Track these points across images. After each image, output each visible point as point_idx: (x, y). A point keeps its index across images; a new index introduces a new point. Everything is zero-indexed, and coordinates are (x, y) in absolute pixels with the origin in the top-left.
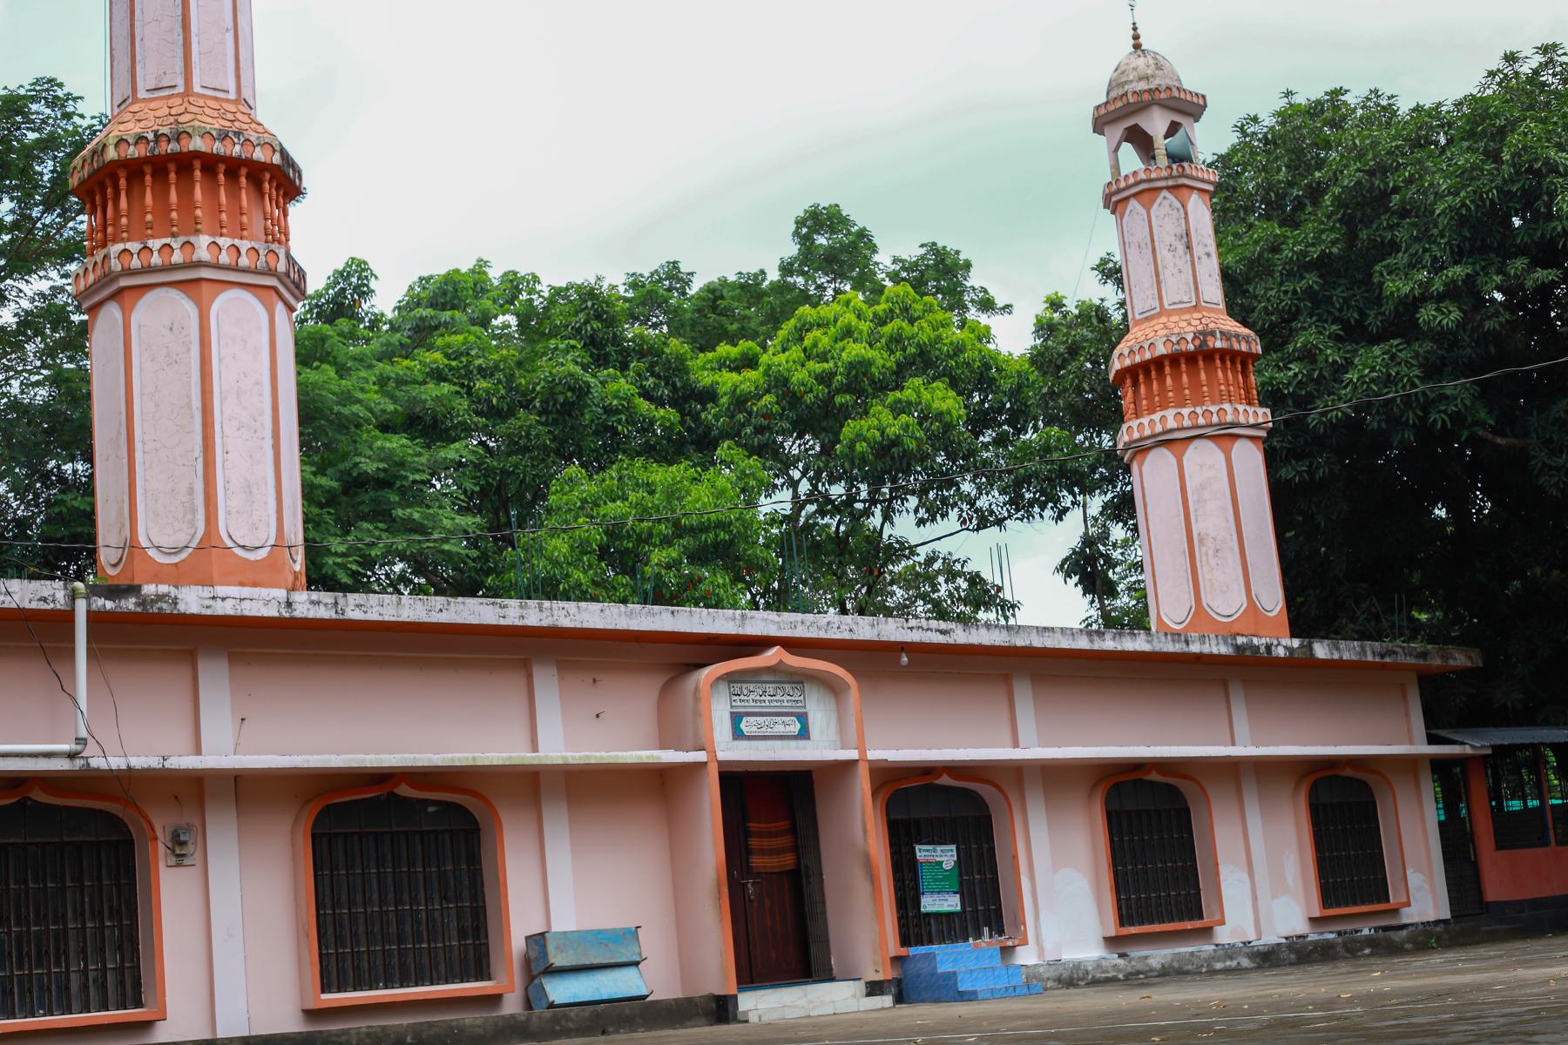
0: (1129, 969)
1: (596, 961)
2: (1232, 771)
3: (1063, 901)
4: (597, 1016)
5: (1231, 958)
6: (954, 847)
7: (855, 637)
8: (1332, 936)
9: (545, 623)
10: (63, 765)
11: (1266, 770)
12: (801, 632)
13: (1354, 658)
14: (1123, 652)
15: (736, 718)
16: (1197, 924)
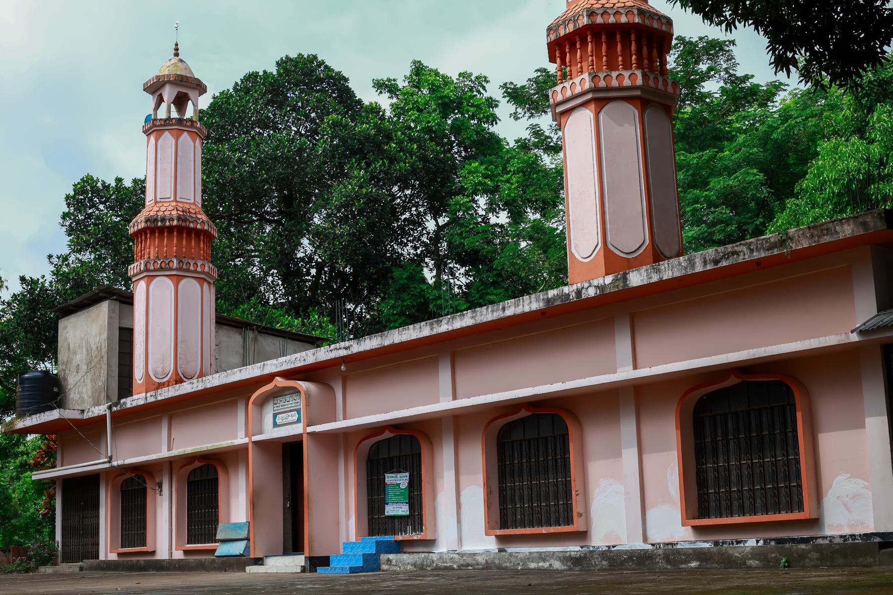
0: (462, 562)
1: (228, 537)
4: (223, 562)
5: (544, 560)
6: (407, 474)
7: (306, 363)
8: (706, 545)
9: (200, 388)
10: (107, 465)
11: (640, 396)
12: (285, 367)
13: (677, 274)
15: (275, 416)
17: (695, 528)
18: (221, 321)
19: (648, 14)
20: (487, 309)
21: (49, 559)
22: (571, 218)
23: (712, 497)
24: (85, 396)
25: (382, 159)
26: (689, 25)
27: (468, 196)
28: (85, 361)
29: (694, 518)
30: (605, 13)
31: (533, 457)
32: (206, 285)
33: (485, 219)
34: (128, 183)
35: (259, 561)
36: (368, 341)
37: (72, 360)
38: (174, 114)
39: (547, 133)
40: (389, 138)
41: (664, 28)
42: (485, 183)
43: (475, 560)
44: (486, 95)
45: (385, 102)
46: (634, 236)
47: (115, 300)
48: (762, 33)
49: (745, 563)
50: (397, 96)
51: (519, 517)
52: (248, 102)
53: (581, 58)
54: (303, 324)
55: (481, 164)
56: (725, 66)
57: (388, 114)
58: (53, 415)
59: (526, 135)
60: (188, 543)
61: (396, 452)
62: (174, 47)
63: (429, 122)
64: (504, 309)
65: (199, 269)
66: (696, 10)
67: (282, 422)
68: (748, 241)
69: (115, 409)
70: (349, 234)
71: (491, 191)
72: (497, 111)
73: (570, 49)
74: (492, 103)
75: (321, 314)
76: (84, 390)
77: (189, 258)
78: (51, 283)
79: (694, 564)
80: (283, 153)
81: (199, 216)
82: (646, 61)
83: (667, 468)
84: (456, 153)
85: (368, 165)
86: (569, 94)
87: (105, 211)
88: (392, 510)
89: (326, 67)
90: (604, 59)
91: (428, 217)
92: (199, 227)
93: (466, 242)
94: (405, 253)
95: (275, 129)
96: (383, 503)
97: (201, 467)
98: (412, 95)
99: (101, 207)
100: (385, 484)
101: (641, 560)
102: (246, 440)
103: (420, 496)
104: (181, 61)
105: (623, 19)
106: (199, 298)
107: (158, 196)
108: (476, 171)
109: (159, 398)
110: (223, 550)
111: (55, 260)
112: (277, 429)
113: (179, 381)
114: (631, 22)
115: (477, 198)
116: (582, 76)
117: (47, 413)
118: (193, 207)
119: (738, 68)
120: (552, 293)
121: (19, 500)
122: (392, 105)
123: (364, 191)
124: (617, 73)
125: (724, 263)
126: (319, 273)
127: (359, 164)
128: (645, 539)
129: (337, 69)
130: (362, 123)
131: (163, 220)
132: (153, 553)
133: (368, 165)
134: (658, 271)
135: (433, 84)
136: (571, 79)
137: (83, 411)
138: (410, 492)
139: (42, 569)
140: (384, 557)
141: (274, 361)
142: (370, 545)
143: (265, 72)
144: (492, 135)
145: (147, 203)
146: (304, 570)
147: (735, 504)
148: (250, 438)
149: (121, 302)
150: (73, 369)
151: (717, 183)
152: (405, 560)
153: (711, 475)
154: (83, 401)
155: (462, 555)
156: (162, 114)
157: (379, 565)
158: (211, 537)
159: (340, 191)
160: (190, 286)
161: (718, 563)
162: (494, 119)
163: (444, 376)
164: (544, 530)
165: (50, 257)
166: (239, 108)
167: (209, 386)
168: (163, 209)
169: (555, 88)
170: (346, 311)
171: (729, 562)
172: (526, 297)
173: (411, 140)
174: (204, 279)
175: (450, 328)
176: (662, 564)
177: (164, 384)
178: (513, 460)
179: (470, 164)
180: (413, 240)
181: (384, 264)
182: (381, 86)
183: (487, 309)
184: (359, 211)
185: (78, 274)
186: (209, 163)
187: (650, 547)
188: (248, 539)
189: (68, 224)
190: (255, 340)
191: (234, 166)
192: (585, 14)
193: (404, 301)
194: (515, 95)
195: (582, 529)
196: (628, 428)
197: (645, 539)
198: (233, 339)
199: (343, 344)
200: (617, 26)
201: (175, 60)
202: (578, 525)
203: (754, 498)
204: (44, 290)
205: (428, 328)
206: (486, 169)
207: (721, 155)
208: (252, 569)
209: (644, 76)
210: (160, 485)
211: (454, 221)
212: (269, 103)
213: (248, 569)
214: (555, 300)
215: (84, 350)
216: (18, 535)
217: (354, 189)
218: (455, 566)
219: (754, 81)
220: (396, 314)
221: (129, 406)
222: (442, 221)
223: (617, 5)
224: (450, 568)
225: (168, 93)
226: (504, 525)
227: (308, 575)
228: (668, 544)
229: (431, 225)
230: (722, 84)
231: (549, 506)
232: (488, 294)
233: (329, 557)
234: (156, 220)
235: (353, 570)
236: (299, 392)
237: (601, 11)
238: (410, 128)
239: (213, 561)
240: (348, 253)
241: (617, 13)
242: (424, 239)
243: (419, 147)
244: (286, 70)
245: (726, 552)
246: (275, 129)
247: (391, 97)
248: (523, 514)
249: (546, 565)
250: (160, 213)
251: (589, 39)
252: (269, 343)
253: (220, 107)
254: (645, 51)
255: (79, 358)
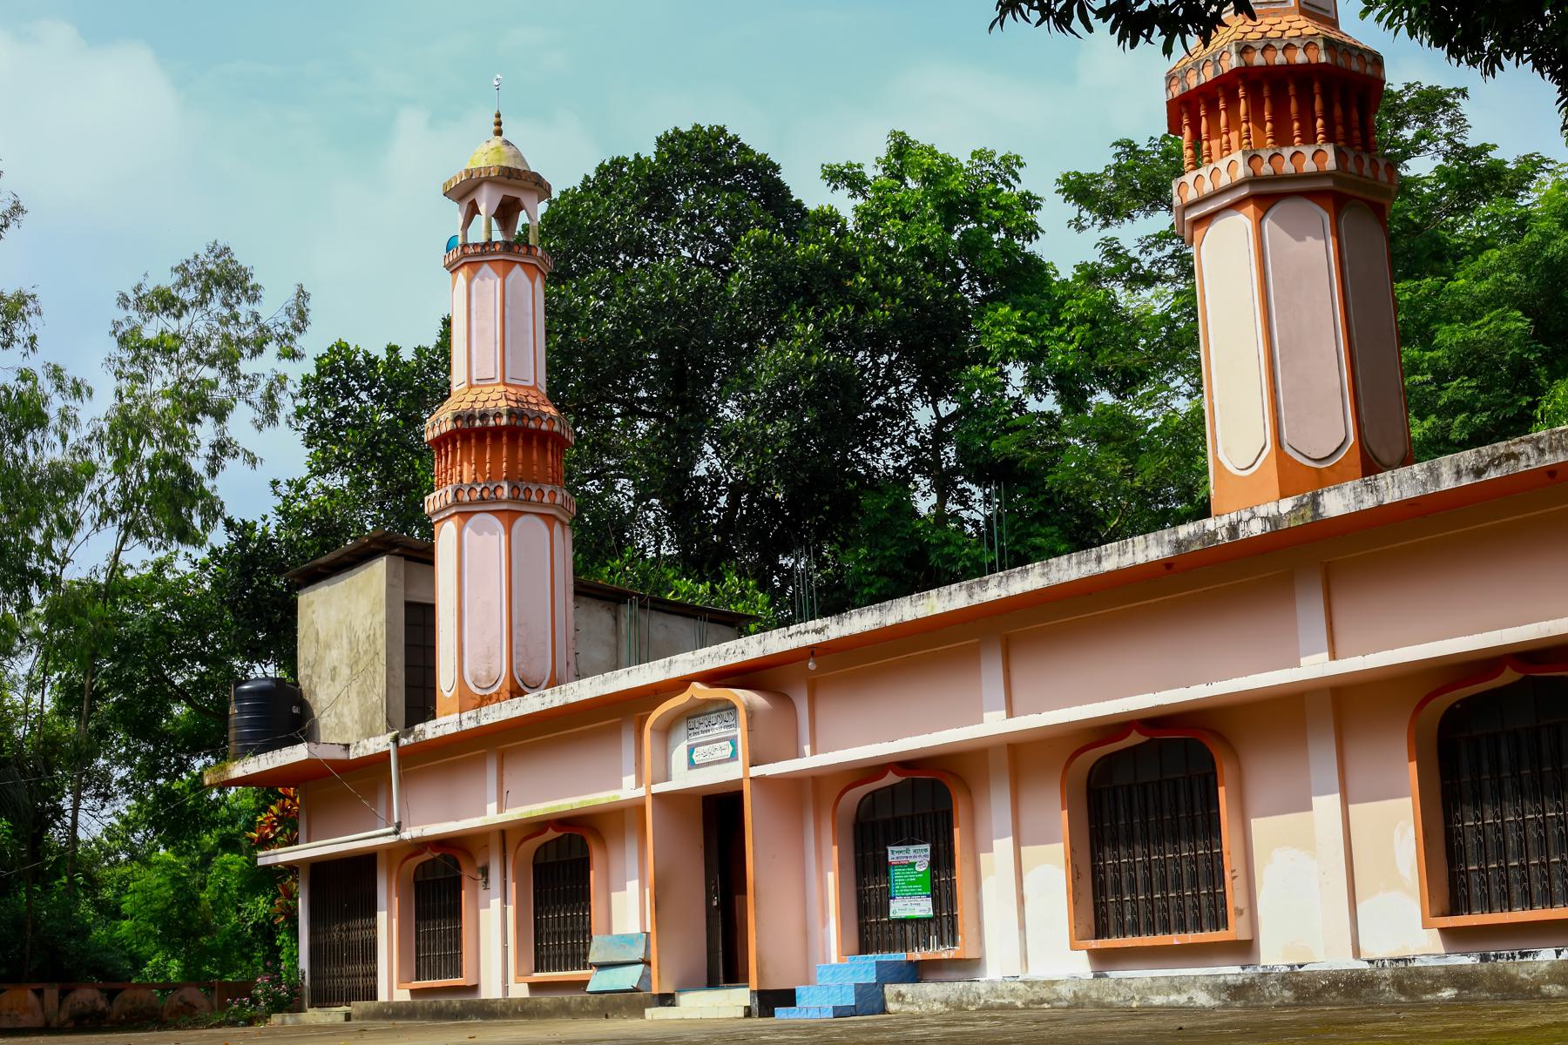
0: (1031, 996)
2: (1283, 717)
3: (494, 927)
4: (602, 1002)
5: (1179, 991)
6: (928, 846)
7: (746, 658)
9: (556, 704)
10: (392, 839)
11: (1345, 707)
12: (709, 665)
13: (1419, 492)
14: (1136, 569)
15: (691, 750)
16: (945, 953)
17: (1446, 933)
18: (585, 591)
19: (1341, 48)
20: (1069, 560)
21: (290, 1003)
22: (1216, 401)
23: (1475, 878)
24: (348, 720)
25: (842, 304)
26: (1411, 63)
27: (993, 365)
28: (346, 661)
29: (1443, 915)
30: (1268, 47)
31: (1152, 815)
32: (557, 527)
33: (1019, 405)
34: (407, 355)
35: (666, 1000)
36: (856, 618)
37: (322, 659)
38: (498, 236)
39: (1134, 253)
40: (853, 266)
41: (1369, 70)
42: (1023, 343)
43: (1054, 992)
44: (1020, 188)
45: (845, 205)
46: (1328, 426)
47: (398, 555)
48: (1547, 75)
49: (1538, 990)
50: (863, 193)
51: (1128, 917)
52: (608, 210)
53: (1227, 125)
54: (713, 591)
55: (1014, 309)
56: (1445, 129)
57: (850, 227)
58: (297, 754)
59: (1094, 256)
60: (536, 971)
61: (909, 811)
62: (494, 119)
63: (922, 238)
64: (1099, 560)
65: (546, 499)
66: (1438, 42)
67: (709, 759)
68: (1534, 435)
69: (404, 742)
70: (790, 435)
71: (1033, 357)
72: (1039, 217)
73: (1207, 110)
74: (1030, 202)
75: (741, 574)
76: (346, 712)
77: (528, 481)
78: (278, 528)
79: (1448, 993)
80: (671, 297)
81: (545, 409)
82: (1340, 129)
83: (1394, 826)
84: (966, 291)
85: (819, 315)
86: (1207, 188)
87: (370, 403)
88: (900, 908)
89: (742, 147)
90: (1269, 126)
91: (918, 403)
92: (544, 427)
93: (994, 446)
94: (880, 466)
95: (653, 255)
96: (886, 896)
97: (557, 839)
98: (891, 190)
99: (363, 396)
100: (887, 864)
101: (1354, 986)
102: (641, 792)
103: (951, 884)
104: (507, 143)
105: (1300, 58)
106: (547, 548)
107: (475, 377)
108: (1008, 322)
109: (484, 722)
110: (600, 981)
111: (284, 489)
112: (695, 771)
113: (516, 692)
114: (1314, 61)
115: (1007, 368)
116: (1231, 157)
117: (286, 750)
118: (533, 393)
119: (1470, 133)
120: (1185, 531)
121: (213, 903)
122: (856, 209)
123: (815, 359)
124: (1292, 150)
125: (1493, 474)
126: (734, 502)
127: (804, 313)
128: (1357, 953)
129: (759, 151)
130: (807, 242)
131: (484, 416)
132: (474, 989)
133: (819, 315)
134: (1375, 489)
135: (929, 171)
136: (1210, 161)
137: (347, 746)
138: (933, 877)
139: (276, 1019)
140: (890, 990)
141: (688, 656)
142: (865, 968)
143: (637, 156)
144: (1030, 259)
145: (454, 389)
146: (748, 1013)
147: (1516, 889)
148: (648, 788)
149: (408, 558)
150: (325, 672)
151: (1449, 335)
152: (926, 998)
153: (1471, 841)
154: (344, 730)
155: (1031, 984)
156: (477, 233)
157: (884, 1003)
158: (578, 958)
159: (771, 361)
160: (532, 529)
161: (1488, 990)
162: (1032, 231)
163: (991, 675)
164: (1176, 939)
165: (275, 483)
166: (593, 220)
167: (572, 700)
168: (483, 397)
169: (1183, 179)
170: (780, 568)
171: (1510, 988)
172: (1139, 539)
173: (893, 269)
174: (555, 518)
175: (1004, 594)
176: (1390, 994)
177: (490, 697)
178: (1117, 820)
179: (996, 310)
180: (892, 443)
181: (843, 484)
182: (838, 176)
183: (1069, 560)
184: (807, 394)
185: (324, 512)
186: (558, 316)
187: (1366, 966)
188: (646, 962)
189: (306, 426)
190: (635, 621)
191: (588, 321)
192: (1233, 49)
193: (884, 548)
194: (1079, 190)
195: (1244, 935)
196: (1322, 759)
197: (1357, 953)
198: (600, 618)
199: (811, 624)
200: (1291, 69)
201: (496, 141)
202: (1236, 929)
203: (1549, 879)
204: (264, 540)
205: (964, 594)
206: (1023, 317)
207: (1452, 285)
208: (655, 1014)
209: (1339, 154)
210: (485, 871)
211: (967, 410)
212: (646, 210)
213: (648, 1012)
214: (1190, 542)
215: (345, 641)
216: (210, 964)
217: (797, 357)
218: (1019, 1004)
219: (1493, 155)
220: (871, 574)
221: (429, 736)
222: (947, 407)
223: (1288, 34)
224: (1011, 1007)
225: (487, 201)
226: (1101, 931)
227: (757, 1021)
228: (1397, 961)
229: (923, 416)
230: (1440, 161)
231: (1182, 898)
232: (1030, 535)
233: (793, 992)
234: (471, 417)
235: (839, 1012)
236: (735, 707)
237: (1261, 45)
238: (889, 250)
239: (583, 1002)
240: (788, 467)
241: (1289, 47)
242: (911, 441)
243: (906, 282)
244: (672, 152)
245: (1505, 972)
246: (653, 255)
247: (853, 196)
248: (1135, 912)
249: (1182, 999)
250: (478, 406)
251: (1241, 93)
252: (660, 626)
253: (562, 220)
254: (1338, 111)
255: (337, 655)
